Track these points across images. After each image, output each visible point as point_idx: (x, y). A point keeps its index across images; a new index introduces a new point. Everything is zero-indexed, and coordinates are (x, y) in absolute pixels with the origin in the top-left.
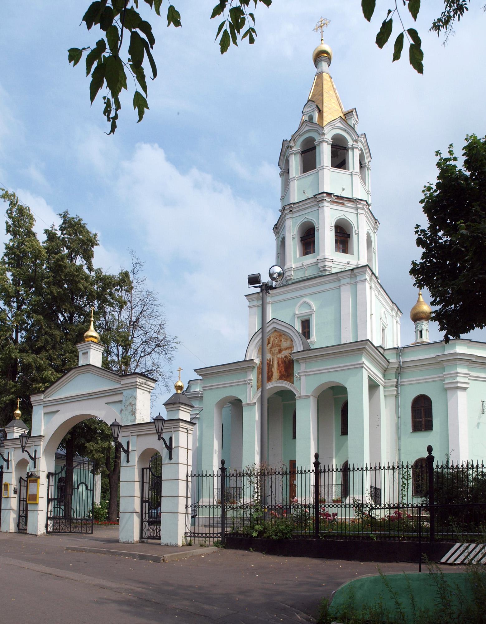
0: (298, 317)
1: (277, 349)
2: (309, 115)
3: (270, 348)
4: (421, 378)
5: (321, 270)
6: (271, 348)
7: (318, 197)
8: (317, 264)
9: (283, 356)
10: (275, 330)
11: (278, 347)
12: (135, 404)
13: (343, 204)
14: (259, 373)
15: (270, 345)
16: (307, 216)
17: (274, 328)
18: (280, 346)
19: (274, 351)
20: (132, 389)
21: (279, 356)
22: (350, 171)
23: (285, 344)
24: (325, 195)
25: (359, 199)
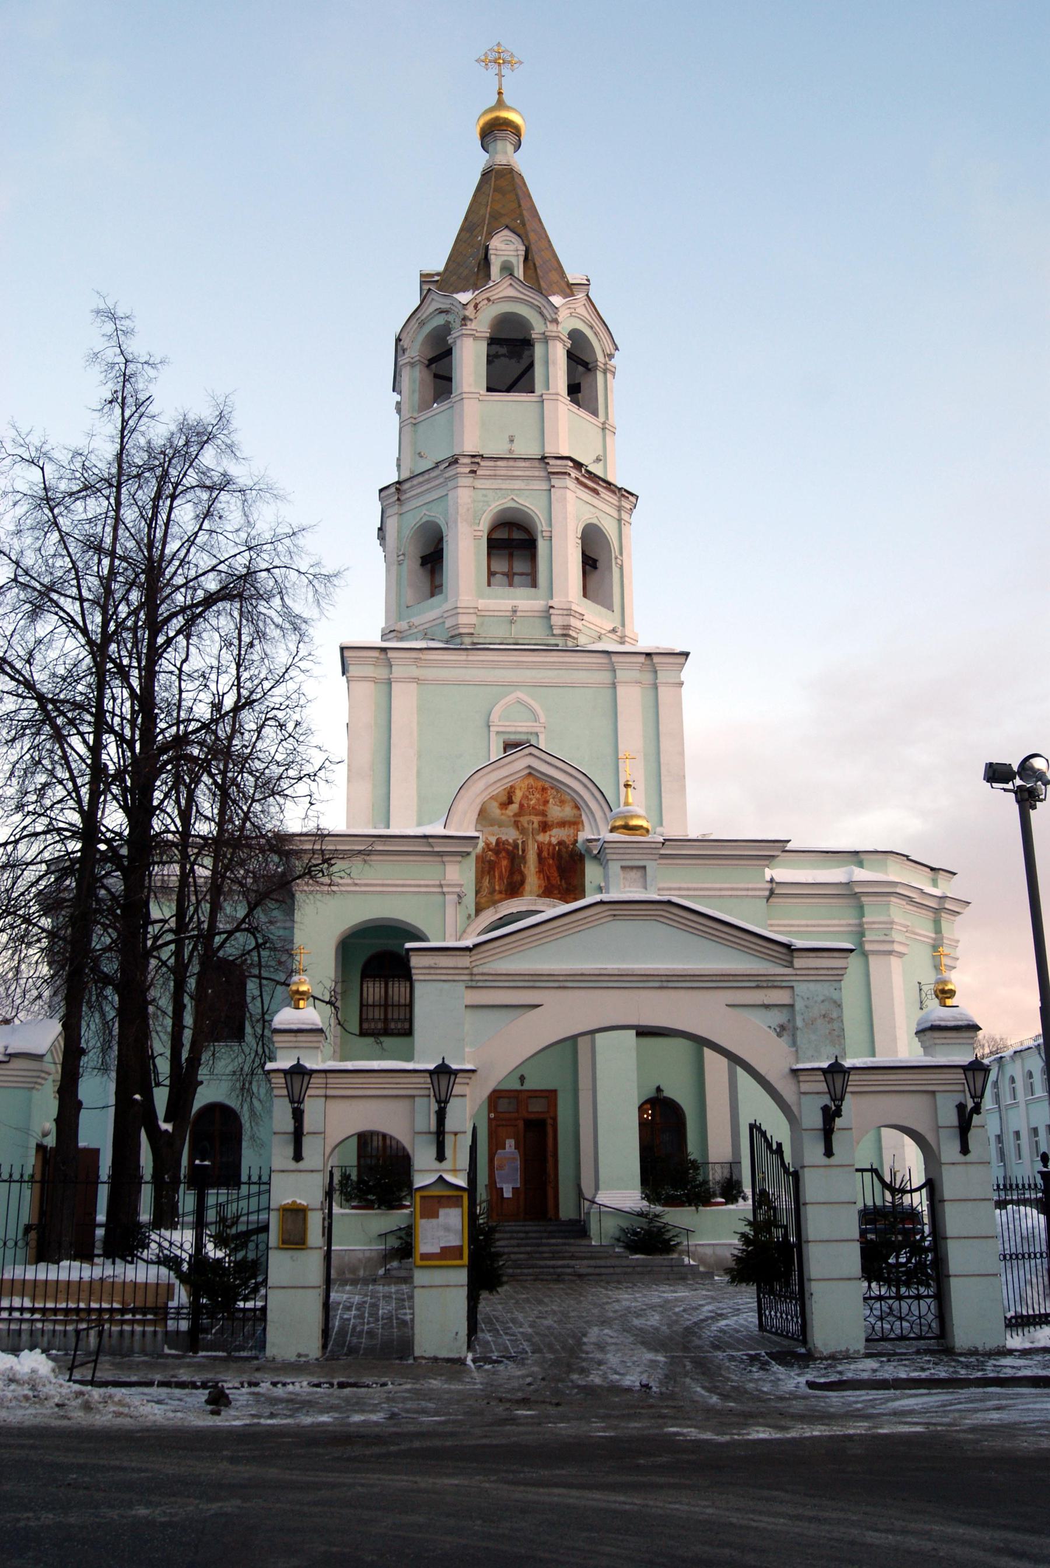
0: (498, 733)
1: (536, 819)
2: (506, 258)
3: (516, 815)
4: (810, 922)
5: (556, 632)
6: (517, 815)
7: (552, 462)
8: (547, 614)
9: (554, 841)
10: (530, 774)
11: (536, 815)
12: (840, 1019)
13: (595, 492)
14: (483, 872)
15: (514, 807)
16: (517, 495)
17: (529, 767)
18: (544, 814)
19: (526, 825)
20: (828, 984)
21: (543, 838)
22: (602, 419)
23: (556, 812)
24: (571, 464)
25: (626, 491)
